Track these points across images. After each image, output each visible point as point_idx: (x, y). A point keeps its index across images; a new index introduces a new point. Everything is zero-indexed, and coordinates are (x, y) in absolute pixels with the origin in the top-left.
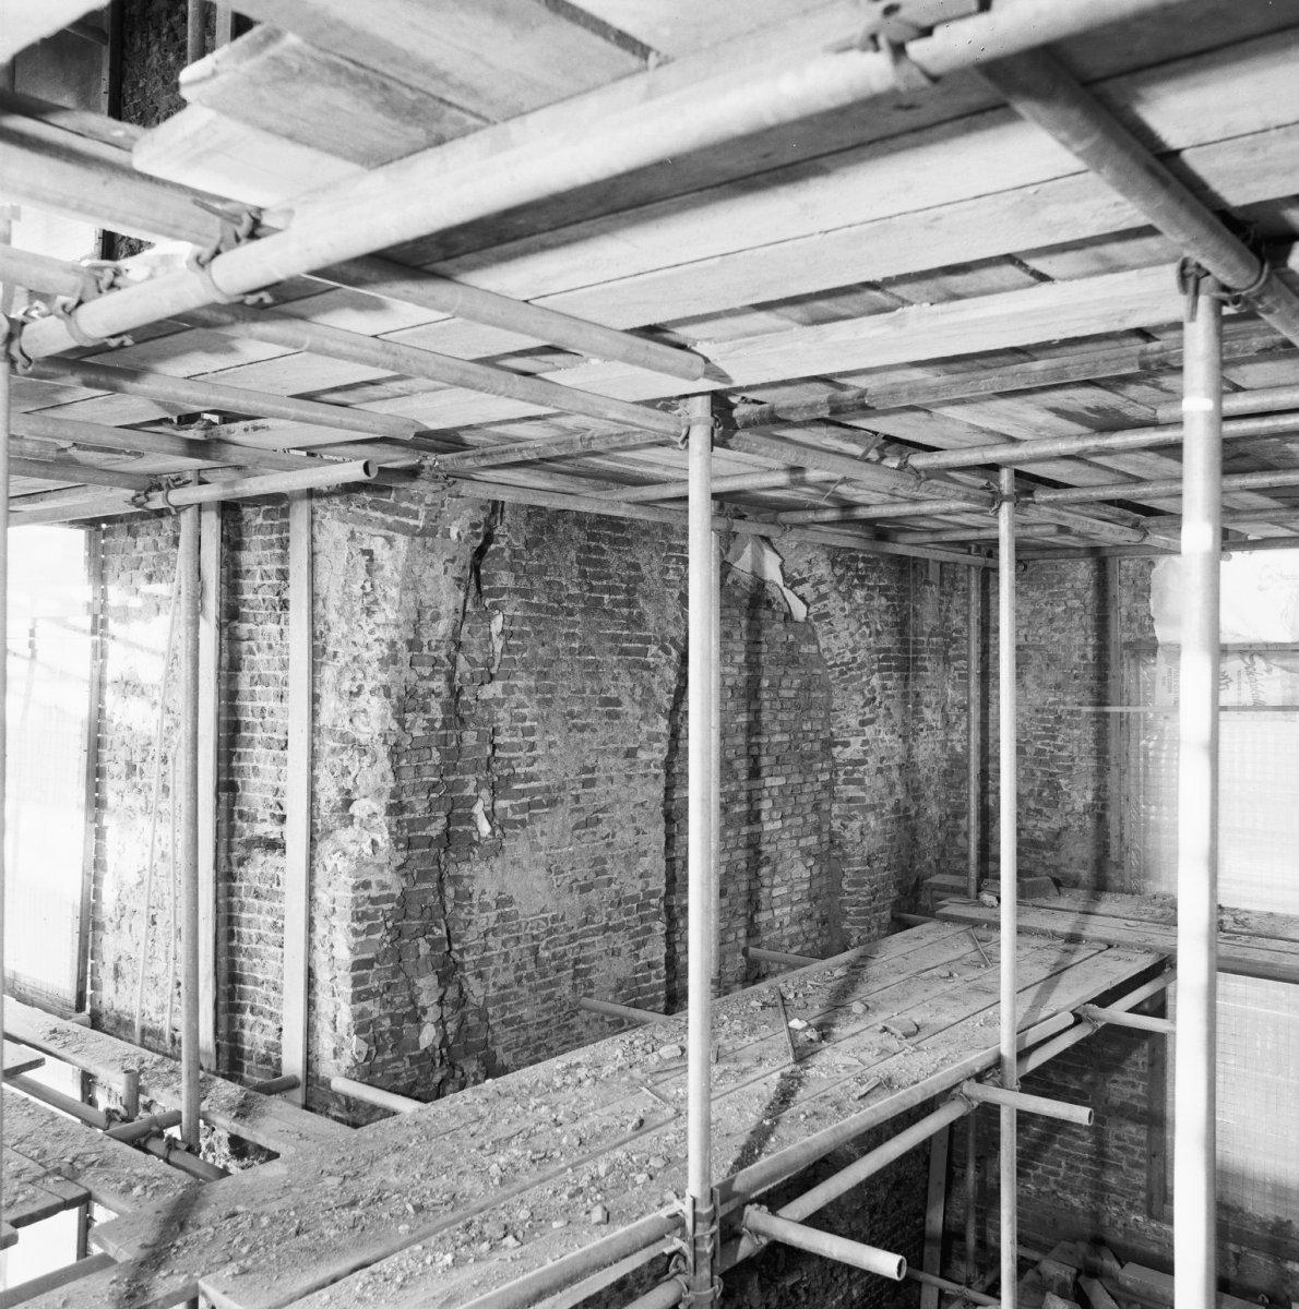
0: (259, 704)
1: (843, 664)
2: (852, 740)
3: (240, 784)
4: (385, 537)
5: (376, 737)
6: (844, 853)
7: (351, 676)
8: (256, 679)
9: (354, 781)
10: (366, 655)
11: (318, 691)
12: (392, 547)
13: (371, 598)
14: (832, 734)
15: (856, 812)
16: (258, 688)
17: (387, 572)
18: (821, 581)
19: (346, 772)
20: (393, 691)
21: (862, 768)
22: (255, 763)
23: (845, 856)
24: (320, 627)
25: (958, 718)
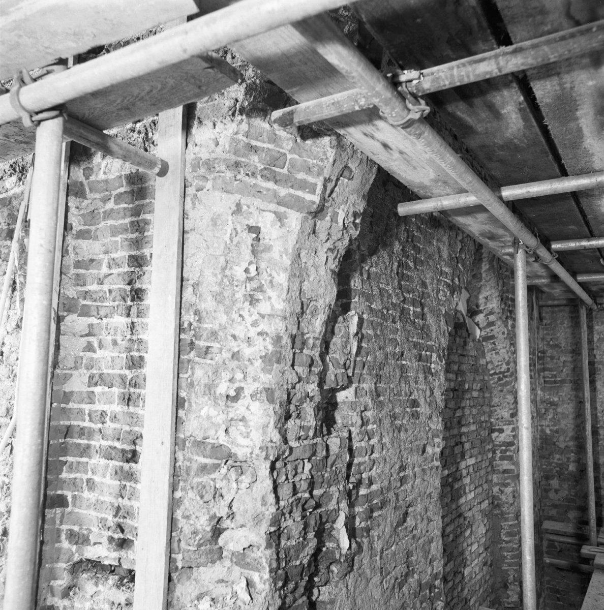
0: (98, 407)
1: (500, 373)
2: (505, 427)
3: (70, 499)
4: (275, 213)
5: (257, 451)
6: (502, 511)
7: (229, 376)
8: (96, 378)
9: (230, 507)
10: (247, 352)
11: (183, 394)
12: (282, 225)
13: (254, 284)
14: (491, 423)
15: (509, 481)
16: (98, 390)
17: (275, 254)
18: (491, 313)
19: (217, 494)
20: (277, 394)
21: (512, 448)
22: (90, 475)
23: (502, 514)
24: (189, 317)
25: (546, 410)
